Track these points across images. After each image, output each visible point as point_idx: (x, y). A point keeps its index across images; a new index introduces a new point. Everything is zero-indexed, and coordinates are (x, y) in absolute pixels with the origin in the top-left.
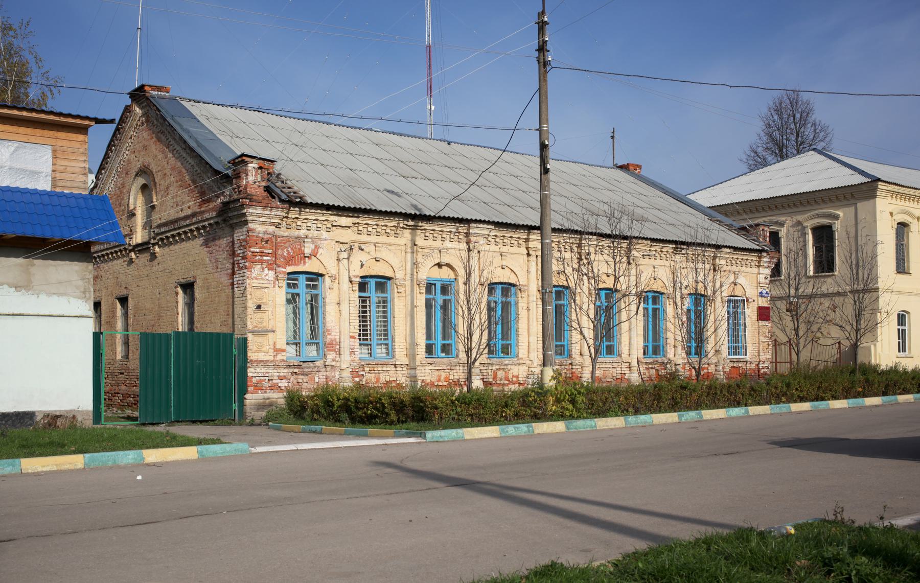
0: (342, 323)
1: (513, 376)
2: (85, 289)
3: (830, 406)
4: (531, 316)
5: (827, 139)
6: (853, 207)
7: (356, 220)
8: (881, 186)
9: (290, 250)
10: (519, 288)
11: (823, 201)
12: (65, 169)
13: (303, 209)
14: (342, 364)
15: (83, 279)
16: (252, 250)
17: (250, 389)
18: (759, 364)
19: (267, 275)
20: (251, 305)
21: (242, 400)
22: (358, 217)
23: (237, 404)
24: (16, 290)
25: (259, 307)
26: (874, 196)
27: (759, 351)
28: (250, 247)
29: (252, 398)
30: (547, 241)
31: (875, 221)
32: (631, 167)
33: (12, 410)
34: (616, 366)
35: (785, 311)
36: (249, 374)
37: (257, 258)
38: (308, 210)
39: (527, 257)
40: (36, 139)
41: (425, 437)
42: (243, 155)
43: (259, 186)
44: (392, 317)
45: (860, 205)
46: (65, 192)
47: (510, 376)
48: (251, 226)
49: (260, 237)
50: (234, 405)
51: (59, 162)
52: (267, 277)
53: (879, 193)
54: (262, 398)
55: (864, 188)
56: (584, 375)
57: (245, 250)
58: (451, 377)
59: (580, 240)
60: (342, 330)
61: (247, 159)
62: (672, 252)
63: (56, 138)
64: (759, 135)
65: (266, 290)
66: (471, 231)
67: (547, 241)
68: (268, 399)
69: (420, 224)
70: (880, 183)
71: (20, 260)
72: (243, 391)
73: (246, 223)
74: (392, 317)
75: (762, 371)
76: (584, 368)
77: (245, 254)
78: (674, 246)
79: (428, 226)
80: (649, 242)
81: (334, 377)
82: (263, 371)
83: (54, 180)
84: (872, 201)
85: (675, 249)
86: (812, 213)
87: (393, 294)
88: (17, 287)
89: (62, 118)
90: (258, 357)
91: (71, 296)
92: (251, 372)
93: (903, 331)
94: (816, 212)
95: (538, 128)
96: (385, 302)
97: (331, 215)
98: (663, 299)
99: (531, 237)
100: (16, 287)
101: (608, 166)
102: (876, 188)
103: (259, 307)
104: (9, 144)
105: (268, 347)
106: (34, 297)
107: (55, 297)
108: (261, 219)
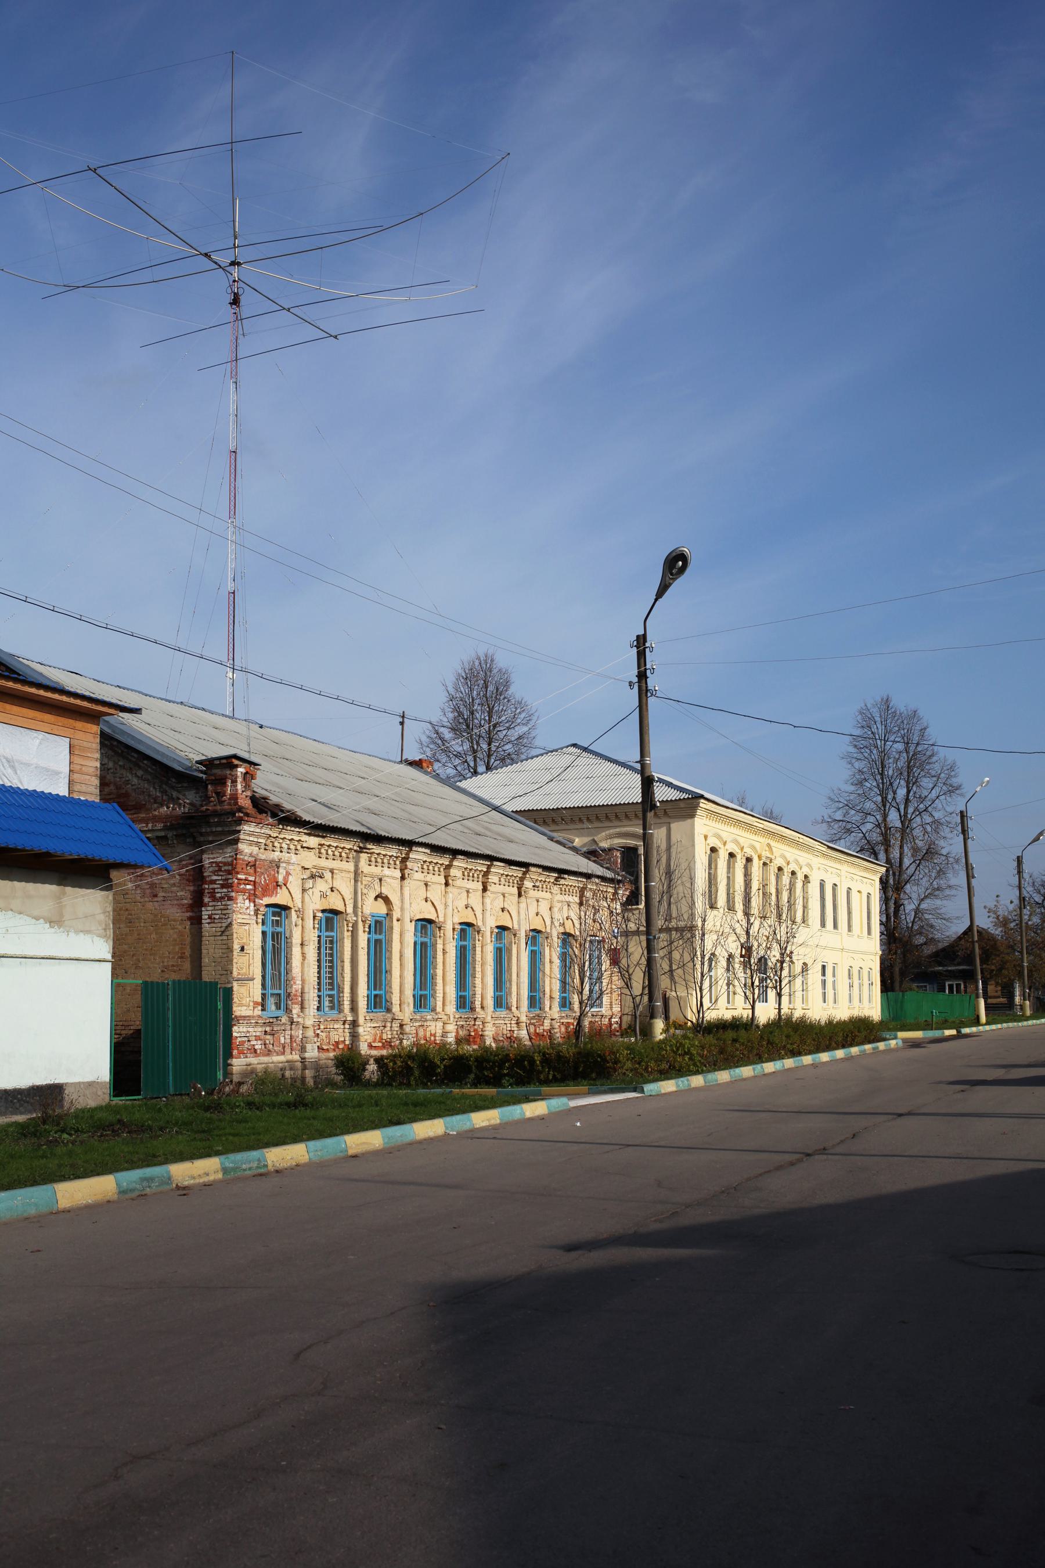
0: (306, 969)
1: (431, 1035)
2: (106, 925)
3: (804, 1061)
4: (448, 960)
5: (532, 723)
6: (665, 828)
7: (323, 841)
8: (703, 803)
9: (266, 876)
10: (438, 926)
11: (627, 816)
12: (81, 769)
13: (285, 827)
14: (306, 1020)
15: (104, 913)
16: (239, 876)
17: (235, 1052)
18: (611, 1018)
19: (247, 908)
20: (236, 947)
21: (227, 1065)
22: (323, 837)
23: (221, 1071)
24: (51, 927)
25: (242, 949)
26: (692, 816)
27: (611, 1002)
28: (238, 873)
29: (238, 1064)
30: (653, 884)
31: (693, 846)
32: (424, 765)
33: (44, 1083)
34: (507, 1022)
35: (739, 957)
36: (235, 1034)
37: (242, 887)
38: (289, 828)
39: (401, 881)
40: (58, 730)
41: (642, 1091)
42: (235, 757)
43: (247, 797)
44: (339, 962)
45: (674, 826)
46: (82, 798)
47: (428, 1035)
48: (241, 846)
49: (245, 861)
50: (218, 1073)
51: (77, 760)
52: (248, 911)
53: (699, 812)
54: (245, 1064)
55: (682, 805)
56: (486, 1033)
57: (230, 877)
58: (385, 1037)
59: (489, 867)
60: (306, 977)
61: (236, 762)
62: (553, 883)
63: (74, 728)
64: (443, 710)
65: (247, 927)
66: (411, 856)
67: (653, 884)
68: (250, 1065)
69: (369, 846)
70: (702, 801)
71: (54, 888)
72: (228, 1055)
73: (236, 841)
74: (339, 962)
75: (613, 1027)
76: (486, 1025)
77: (230, 881)
78: (556, 875)
79: (376, 849)
80: (540, 870)
81: (298, 1037)
82: (245, 1030)
83: (71, 783)
84: (689, 821)
85: (557, 879)
86: (611, 831)
87: (342, 933)
88: (52, 922)
89: (72, 699)
90: (242, 1012)
91: (95, 934)
92: (237, 1031)
93: (825, 980)
94: (618, 830)
95: (638, 759)
96: (331, 942)
97: (305, 834)
98: (540, 939)
99: (455, 863)
100: (50, 922)
101: (394, 759)
102: (698, 805)
103: (242, 949)
104: (35, 735)
105: (248, 999)
106: (64, 935)
107: (81, 934)
108: (251, 839)
